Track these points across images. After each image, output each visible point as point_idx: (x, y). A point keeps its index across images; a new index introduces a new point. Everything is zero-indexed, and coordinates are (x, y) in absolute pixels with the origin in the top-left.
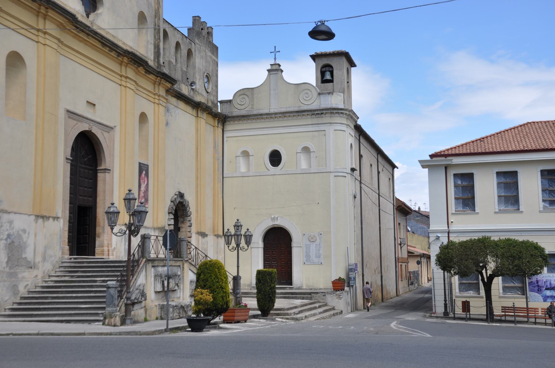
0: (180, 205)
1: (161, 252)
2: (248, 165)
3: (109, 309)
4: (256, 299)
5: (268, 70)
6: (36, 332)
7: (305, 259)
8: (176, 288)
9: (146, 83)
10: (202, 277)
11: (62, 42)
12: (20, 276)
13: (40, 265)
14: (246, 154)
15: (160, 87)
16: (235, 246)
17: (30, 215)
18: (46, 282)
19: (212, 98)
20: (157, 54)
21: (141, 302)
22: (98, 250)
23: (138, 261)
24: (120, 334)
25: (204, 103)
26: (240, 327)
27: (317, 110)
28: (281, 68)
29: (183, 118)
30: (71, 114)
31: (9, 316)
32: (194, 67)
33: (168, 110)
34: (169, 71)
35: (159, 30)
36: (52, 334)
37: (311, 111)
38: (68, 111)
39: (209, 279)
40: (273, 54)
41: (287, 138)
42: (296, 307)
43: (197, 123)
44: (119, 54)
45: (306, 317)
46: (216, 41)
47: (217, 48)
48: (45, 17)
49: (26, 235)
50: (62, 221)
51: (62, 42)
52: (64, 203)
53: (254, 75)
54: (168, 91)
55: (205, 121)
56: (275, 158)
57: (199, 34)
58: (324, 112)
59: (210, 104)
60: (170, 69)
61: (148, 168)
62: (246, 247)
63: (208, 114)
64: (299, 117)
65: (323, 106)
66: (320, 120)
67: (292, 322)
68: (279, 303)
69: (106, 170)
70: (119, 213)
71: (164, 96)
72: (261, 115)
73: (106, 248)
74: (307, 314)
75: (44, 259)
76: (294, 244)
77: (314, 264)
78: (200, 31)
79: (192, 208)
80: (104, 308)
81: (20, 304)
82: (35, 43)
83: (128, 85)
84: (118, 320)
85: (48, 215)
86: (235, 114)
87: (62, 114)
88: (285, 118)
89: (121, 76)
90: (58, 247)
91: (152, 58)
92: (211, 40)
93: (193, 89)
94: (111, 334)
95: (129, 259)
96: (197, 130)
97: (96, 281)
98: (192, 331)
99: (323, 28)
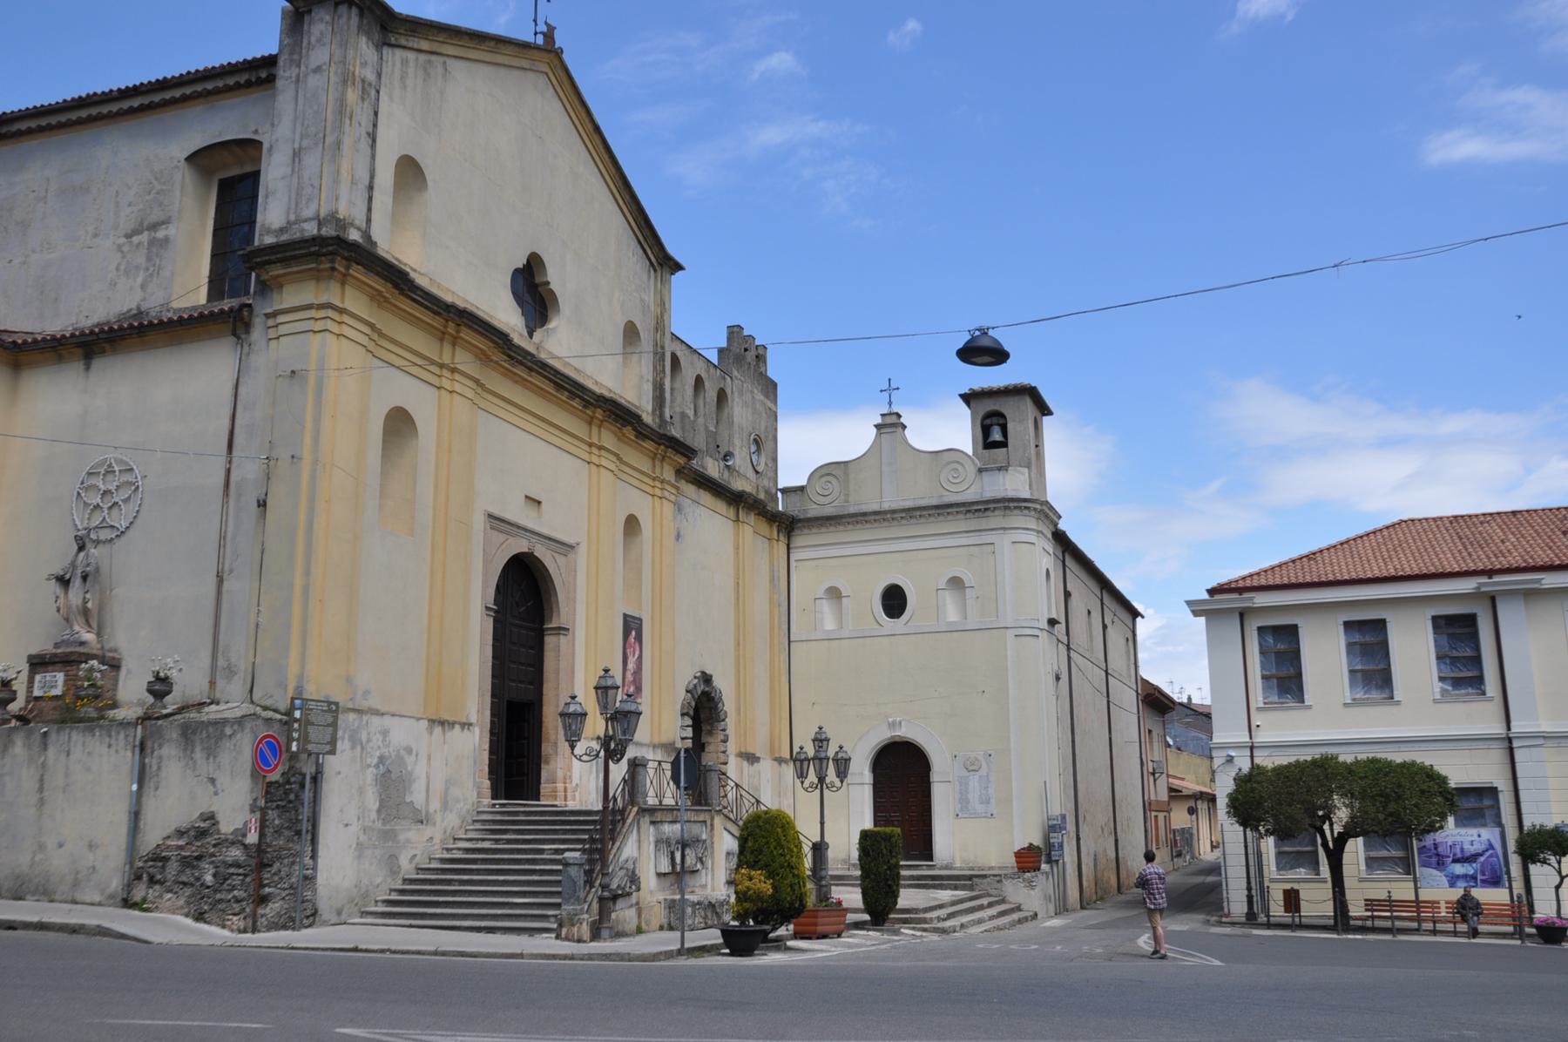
1: (668, 794)
3: (568, 908)
6: (432, 948)
8: (699, 866)
11: (482, 386)
12: (402, 837)
13: (438, 817)
17: (419, 719)
18: (448, 850)
19: (766, 482)
22: (545, 788)
23: (622, 812)
24: (590, 957)
29: (710, 524)
34: (684, 437)
36: (462, 954)
37: (963, 504)
38: (490, 516)
40: (886, 394)
41: (917, 561)
42: (941, 906)
43: (737, 534)
44: (587, 404)
45: (962, 926)
47: (775, 385)
49: (413, 758)
51: (482, 386)
52: (481, 695)
53: (849, 437)
54: (680, 472)
55: (752, 532)
56: (894, 601)
57: (739, 360)
59: (762, 496)
60: (683, 428)
62: (838, 784)
65: (988, 495)
66: (983, 523)
67: (935, 937)
68: (907, 898)
69: (561, 630)
72: (864, 514)
73: (560, 786)
75: (445, 806)
76: (935, 776)
77: (976, 816)
78: (742, 353)
79: (729, 704)
80: (558, 906)
81: (402, 892)
84: (585, 930)
86: (811, 514)
87: (479, 522)
90: (471, 784)
91: (650, 408)
94: (572, 958)
95: (605, 808)
97: (541, 851)
98: (731, 954)
99: (985, 342)
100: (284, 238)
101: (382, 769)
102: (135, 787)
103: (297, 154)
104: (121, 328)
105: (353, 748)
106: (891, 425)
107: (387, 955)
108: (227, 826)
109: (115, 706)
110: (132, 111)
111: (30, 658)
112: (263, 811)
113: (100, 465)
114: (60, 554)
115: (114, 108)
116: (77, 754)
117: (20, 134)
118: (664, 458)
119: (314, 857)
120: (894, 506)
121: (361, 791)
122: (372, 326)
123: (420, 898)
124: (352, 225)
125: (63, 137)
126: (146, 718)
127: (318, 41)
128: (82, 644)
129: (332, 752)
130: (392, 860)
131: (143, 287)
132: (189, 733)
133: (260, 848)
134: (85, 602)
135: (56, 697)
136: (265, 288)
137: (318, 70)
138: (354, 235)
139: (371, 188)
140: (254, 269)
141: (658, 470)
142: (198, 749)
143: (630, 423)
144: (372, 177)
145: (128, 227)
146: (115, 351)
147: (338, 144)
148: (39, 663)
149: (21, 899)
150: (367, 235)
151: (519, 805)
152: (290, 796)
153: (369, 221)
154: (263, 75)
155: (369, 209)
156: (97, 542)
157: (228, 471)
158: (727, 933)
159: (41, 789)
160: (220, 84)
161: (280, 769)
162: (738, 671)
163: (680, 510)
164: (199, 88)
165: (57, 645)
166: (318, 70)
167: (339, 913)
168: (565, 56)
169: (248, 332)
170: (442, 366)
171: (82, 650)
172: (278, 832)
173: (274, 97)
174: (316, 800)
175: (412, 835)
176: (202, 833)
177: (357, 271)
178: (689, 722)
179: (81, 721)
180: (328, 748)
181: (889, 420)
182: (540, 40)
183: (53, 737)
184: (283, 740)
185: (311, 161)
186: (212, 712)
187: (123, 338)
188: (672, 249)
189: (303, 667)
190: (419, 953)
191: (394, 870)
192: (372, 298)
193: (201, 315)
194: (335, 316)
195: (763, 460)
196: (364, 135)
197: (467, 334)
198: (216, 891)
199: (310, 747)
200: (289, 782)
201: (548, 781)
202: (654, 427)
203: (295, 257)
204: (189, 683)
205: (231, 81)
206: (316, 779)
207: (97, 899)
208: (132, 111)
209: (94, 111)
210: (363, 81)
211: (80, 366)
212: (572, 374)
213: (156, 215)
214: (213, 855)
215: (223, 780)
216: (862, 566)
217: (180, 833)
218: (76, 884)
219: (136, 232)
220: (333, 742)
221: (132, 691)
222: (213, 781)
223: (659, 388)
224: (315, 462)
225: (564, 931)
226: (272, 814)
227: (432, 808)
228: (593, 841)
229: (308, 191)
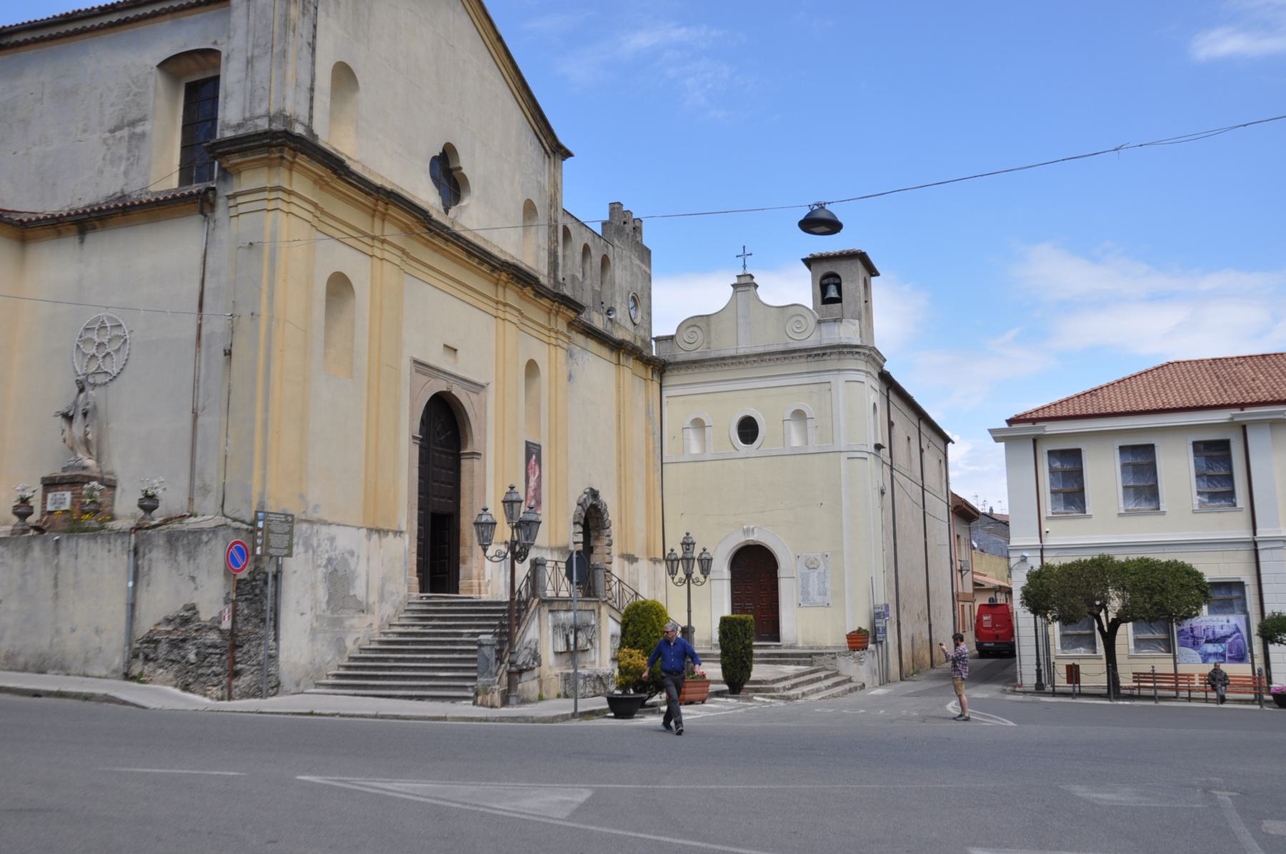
1: (564, 588)
6: (373, 713)
8: (589, 646)
9: (536, 313)
12: (347, 623)
13: (376, 607)
17: (359, 528)
18: (385, 634)
19: (642, 333)
20: (554, 265)
21: (532, 669)
24: (501, 719)
29: (596, 368)
30: (420, 366)
32: (613, 284)
34: (575, 294)
36: (397, 717)
37: (805, 350)
38: (416, 362)
40: (741, 259)
41: (764, 397)
42: (786, 679)
44: (494, 269)
45: (804, 694)
46: (647, 241)
47: (649, 252)
52: (410, 508)
54: (571, 324)
55: (630, 372)
56: (748, 430)
57: (620, 231)
59: (639, 344)
60: (573, 288)
62: (702, 578)
65: (826, 342)
67: (781, 703)
68: (759, 672)
69: (474, 455)
70: (495, 523)
72: (723, 358)
73: (475, 582)
74: (806, 689)
75: (382, 598)
76: (782, 573)
77: (815, 605)
78: (623, 226)
79: (612, 514)
80: (474, 678)
81: (348, 668)
83: (508, 317)
84: (497, 698)
85: (386, 528)
86: (680, 359)
87: (406, 366)
89: (497, 303)
91: (546, 272)
94: (486, 720)
95: (512, 599)
97: (460, 635)
98: (616, 717)
99: (822, 215)
100: (241, 132)
102: (131, 584)
103: (250, 62)
104: (108, 209)
105: (306, 552)
106: (745, 284)
107: (337, 718)
108: (205, 615)
109: (113, 518)
110: (111, 25)
112: (235, 603)
114: (64, 395)
116: (84, 557)
117: (18, 45)
118: (558, 312)
119: (276, 639)
120: (748, 352)
121: (313, 586)
122: (315, 205)
123: (362, 673)
124: (297, 120)
125: (55, 47)
126: (138, 528)
128: (85, 468)
129: (290, 555)
130: (339, 643)
131: (126, 173)
132: (173, 540)
133: (233, 633)
136: (226, 174)
138: (299, 130)
139: (312, 89)
140: (218, 158)
142: (180, 553)
144: (313, 80)
145: (111, 124)
146: (104, 227)
147: (284, 53)
148: (50, 484)
149: (43, 672)
150: (309, 129)
152: (256, 592)
153: (311, 117)
155: (311, 108)
156: (94, 385)
157: (200, 326)
158: (612, 700)
159: (56, 586)
161: (247, 570)
167: (298, 685)
169: (213, 211)
170: (373, 238)
171: (84, 473)
172: (247, 620)
173: (229, 13)
174: (277, 594)
176: (186, 621)
177: (302, 160)
178: (581, 529)
179: (86, 530)
180: (286, 551)
181: (744, 280)
183: (64, 544)
184: (249, 545)
185: (262, 66)
186: (191, 523)
190: (362, 716)
191: (341, 649)
192: (315, 182)
193: (174, 197)
195: (640, 314)
197: (393, 211)
198: (198, 667)
199: (271, 551)
200: (254, 580)
204: (172, 500)
206: (276, 577)
207: (104, 673)
208: (111, 25)
209: (79, 26)
211: (76, 240)
213: (134, 114)
214: (195, 638)
215: (202, 577)
216: (722, 402)
217: (168, 621)
218: (86, 661)
219: (118, 128)
220: (290, 547)
221: (126, 507)
222: (193, 578)
223: (553, 255)
224: (271, 318)
225: (480, 698)
226: (242, 605)
228: (502, 626)
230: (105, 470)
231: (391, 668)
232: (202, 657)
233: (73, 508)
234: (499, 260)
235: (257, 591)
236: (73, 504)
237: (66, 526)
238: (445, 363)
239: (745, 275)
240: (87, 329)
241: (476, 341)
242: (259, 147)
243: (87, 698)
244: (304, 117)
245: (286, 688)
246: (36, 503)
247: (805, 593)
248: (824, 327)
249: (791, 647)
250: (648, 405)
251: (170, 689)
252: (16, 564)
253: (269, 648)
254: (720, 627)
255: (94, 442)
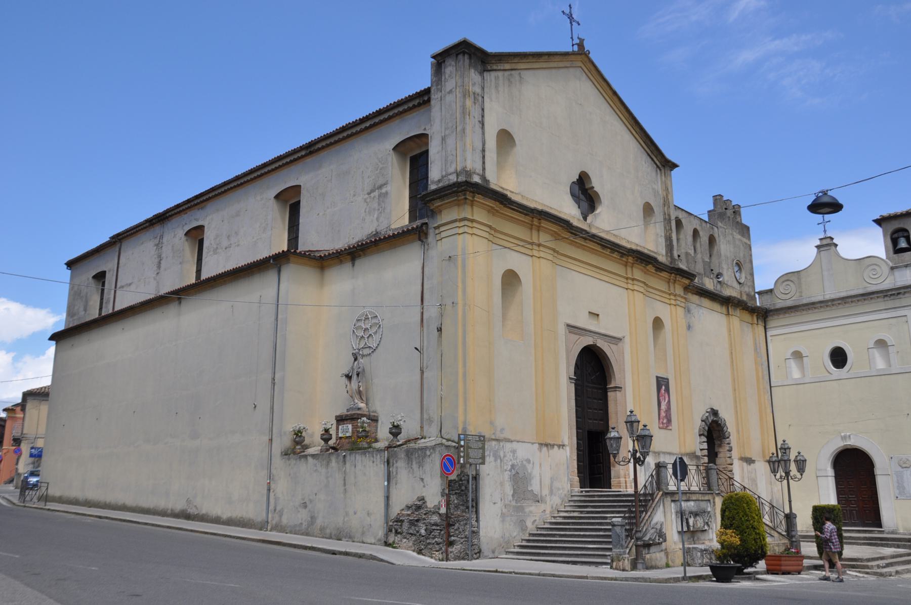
0: (714, 425)
1: (694, 484)
2: (802, 368)
3: (616, 551)
4: (815, 544)
5: (817, 247)
6: (537, 572)
7: (897, 491)
8: (706, 528)
9: (658, 283)
10: (727, 514)
11: (557, 252)
12: (527, 510)
13: (548, 498)
14: (798, 355)
15: (676, 286)
16: (784, 474)
17: (533, 444)
18: (554, 517)
19: (747, 289)
20: (670, 247)
21: (659, 544)
22: (614, 481)
23: (652, 495)
24: (626, 579)
25: (735, 297)
26: (782, 579)
27: (892, 290)
28: (834, 241)
29: (710, 320)
30: (572, 328)
31: (518, 553)
32: (719, 255)
33: (689, 311)
34: (687, 267)
35: (670, 220)
36: (554, 576)
37: (881, 292)
38: (568, 325)
39: (737, 518)
40: (821, 226)
41: (854, 332)
42: (882, 558)
43: (729, 323)
44: (622, 255)
45: (897, 572)
46: (745, 220)
47: (748, 228)
48: (539, 229)
49: (531, 465)
50: (568, 449)
51: (557, 252)
52: (570, 429)
53: (800, 254)
54: (686, 289)
55: (738, 321)
56: (839, 357)
57: (722, 216)
58: (902, 291)
59: (745, 298)
60: (687, 261)
61: (668, 382)
62: (799, 475)
63: (743, 309)
64: (866, 302)
65: (900, 284)
66: (897, 303)
67: (872, 578)
68: (849, 551)
69: (617, 388)
70: (621, 438)
71: (682, 294)
72: (813, 303)
73: (622, 479)
74: (899, 568)
75: (551, 492)
76: (878, 471)
78: (725, 212)
79: (731, 427)
80: (610, 549)
81: (528, 541)
82: (530, 258)
83: (636, 288)
84: (627, 564)
85: (552, 443)
86: (778, 306)
87: (562, 330)
88: (847, 305)
89: (627, 279)
90: (566, 479)
91: (664, 252)
92: (738, 220)
93: (720, 282)
94: (616, 579)
95: (636, 492)
96: (730, 331)
97: (606, 518)
98: (717, 581)
99: (825, 200)
100: (441, 185)
101: (514, 472)
102: (386, 483)
103: (444, 139)
104: (367, 243)
105: (495, 460)
106: (827, 245)
107: (513, 575)
108: (431, 503)
109: (376, 441)
110: (367, 129)
111: (337, 417)
112: (448, 496)
113: (362, 315)
114: (346, 364)
115: (358, 128)
116: (359, 466)
117: (319, 149)
118: (675, 281)
119: (477, 521)
120: (833, 297)
121: (502, 484)
122: (490, 227)
123: (538, 545)
124: (474, 173)
125: (337, 147)
126: (389, 447)
127: (450, 76)
128: (359, 409)
129: (483, 463)
130: (522, 523)
131: (377, 219)
132: (409, 454)
133: (447, 516)
134: (359, 387)
135: (347, 437)
136: (433, 214)
137: (450, 92)
138: (476, 179)
139: (483, 151)
140: (431, 201)
141: (672, 288)
142: (414, 463)
143: (650, 263)
144: (484, 145)
145: (368, 189)
146: (365, 255)
147: (464, 130)
148: (340, 420)
149: (340, 540)
150: (483, 177)
151: (597, 492)
152: (463, 490)
153: (484, 169)
154: (426, 98)
155: (484, 163)
156: (363, 356)
157: (422, 313)
158: (713, 568)
159: (345, 485)
160: (406, 107)
161: (456, 473)
162: (736, 407)
163: (689, 311)
164: (396, 111)
165: (348, 410)
166: (450, 92)
167: (493, 552)
168: (590, 55)
169: (426, 238)
170: (532, 244)
171: (359, 412)
172: (457, 507)
173: (430, 111)
174: (476, 490)
175: (532, 508)
176: (419, 508)
177: (479, 198)
178: (705, 439)
179: (360, 449)
180: (480, 461)
181: (825, 242)
182: (576, 48)
183: (348, 458)
184: (456, 457)
185: (450, 141)
186: (422, 443)
187: (368, 248)
188: (669, 156)
189: (466, 417)
190: (530, 574)
191: (523, 528)
192: (489, 211)
193: (408, 230)
194: (469, 224)
195: (743, 275)
196: (477, 123)
197: (544, 224)
198: (427, 538)
199: (470, 461)
200: (461, 480)
201: (615, 477)
202: (668, 263)
203: (446, 195)
204: (410, 428)
205: (411, 105)
206: (476, 478)
207: (373, 541)
208: (367, 129)
209: (349, 132)
210: (474, 93)
211: (350, 264)
212: (612, 239)
213: (380, 182)
214: (424, 519)
215: (427, 479)
216: (815, 337)
217: (408, 507)
218: (363, 533)
219: (372, 191)
220: (483, 458)
221: (383, 432)
222: (422, 479)
223: (669, 239)
224: (465, 305)
225: (614, 564)
226: (453, 498)
227: (544, 494)
228: (632, 512)
229: (450, 158)
230: (371, 410)
231: (556, 542)
232: (429, 532)
233: (354, 435)
234: (626, 248)
235: (463, 488)
236: (353, 432)
237: (348, 446)
238: (591, 325)
239: (826, 238)
240: (358, 320)
241: (613, 307)
242: (450, 194)
243: (360, 556)
244: (479, 169)
245: (486, 553)
246: (333, 432)
247: (901, 487)
248: (897, 273)
249: (893, 533)
250: (755, 344)
251: (411, 552)
252: (323, 471)
253: (472, 526)
254: (813, 514)
255: (364, 392)
